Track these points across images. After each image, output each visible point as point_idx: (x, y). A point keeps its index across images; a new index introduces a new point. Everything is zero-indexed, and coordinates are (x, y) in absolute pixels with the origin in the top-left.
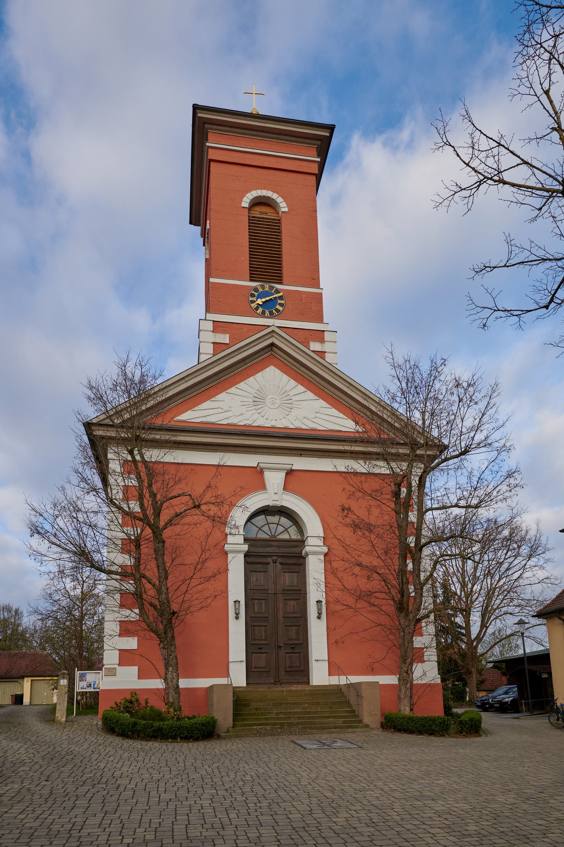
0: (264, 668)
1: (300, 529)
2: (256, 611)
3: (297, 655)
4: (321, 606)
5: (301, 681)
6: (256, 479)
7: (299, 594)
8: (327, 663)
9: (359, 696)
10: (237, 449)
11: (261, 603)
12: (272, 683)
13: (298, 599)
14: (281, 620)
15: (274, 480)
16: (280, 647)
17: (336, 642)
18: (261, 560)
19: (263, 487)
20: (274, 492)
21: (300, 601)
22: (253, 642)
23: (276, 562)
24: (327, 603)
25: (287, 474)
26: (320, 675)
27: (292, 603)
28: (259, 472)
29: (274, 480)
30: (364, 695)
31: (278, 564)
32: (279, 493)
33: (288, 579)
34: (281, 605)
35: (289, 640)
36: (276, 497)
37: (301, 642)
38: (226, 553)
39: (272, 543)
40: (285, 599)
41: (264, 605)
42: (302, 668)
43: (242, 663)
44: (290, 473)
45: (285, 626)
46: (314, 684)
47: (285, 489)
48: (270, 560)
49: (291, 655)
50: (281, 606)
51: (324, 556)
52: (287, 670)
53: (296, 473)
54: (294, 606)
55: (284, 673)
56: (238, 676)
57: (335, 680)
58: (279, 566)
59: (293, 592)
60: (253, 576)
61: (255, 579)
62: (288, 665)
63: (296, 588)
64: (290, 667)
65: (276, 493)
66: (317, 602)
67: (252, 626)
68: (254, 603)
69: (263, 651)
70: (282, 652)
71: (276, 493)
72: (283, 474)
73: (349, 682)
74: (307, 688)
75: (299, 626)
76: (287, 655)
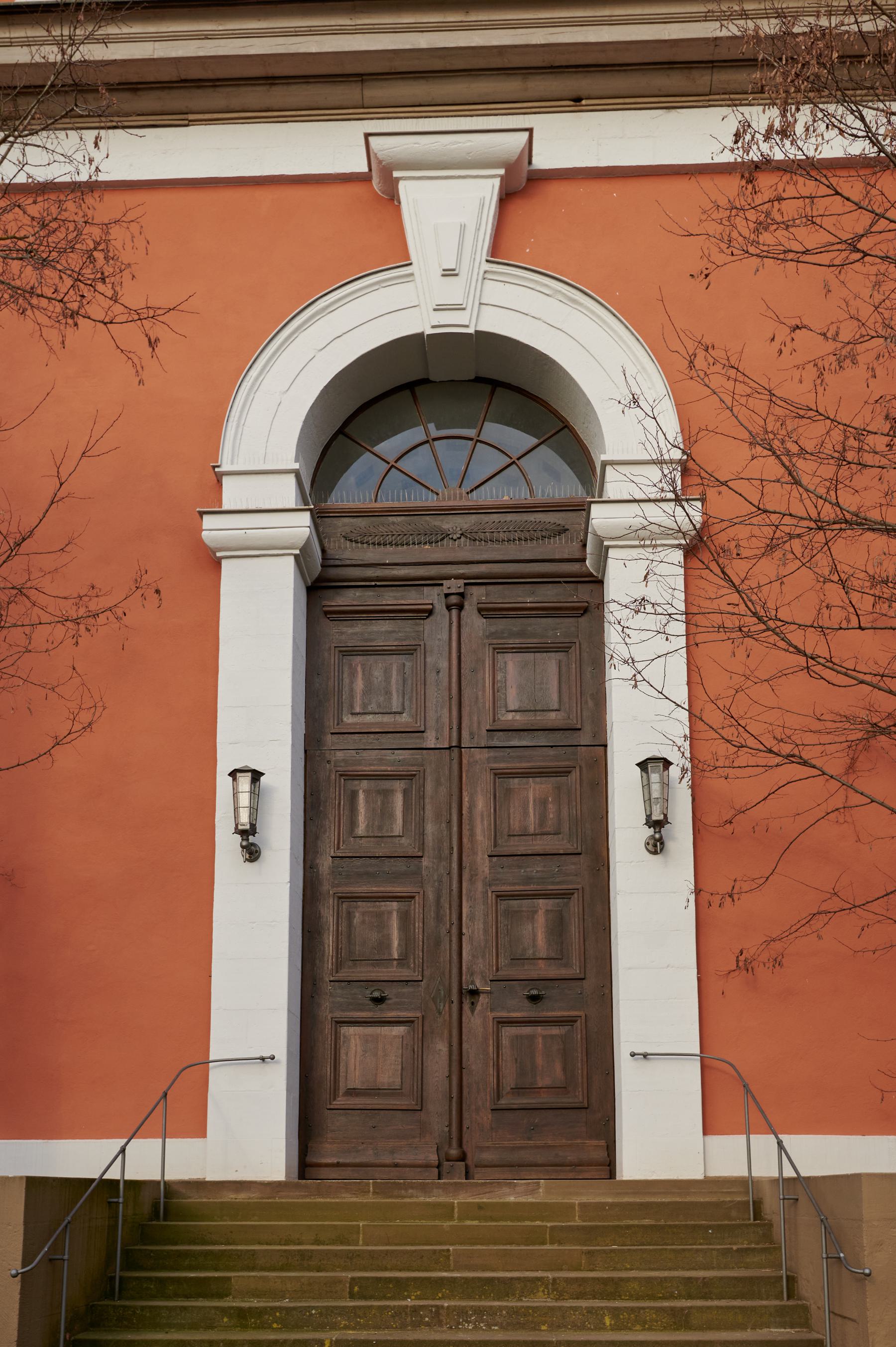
0: (392, 1092)
1: (584, 464)
2: (361, 829)
3: (555, 1031)
4: (665, 785)
5: (571, 1157)
6: (365, 220)
7: (573, 750)
8: (695, 1068)
9: (840, 1261)
10: (280, 95)
11: (387, 794)
12: (427, 1166)
13: (566, 772)
14: (484, 866)
15: (447, 212)
16: (475, 993)
17: (745, 965)
18: (389, 598)
19: (396, 254)
20: (445, 272)
21: (575, 775)
22: (343, 974)
23: (460, 607)
24: (698, 769)
25: (507, 197)
26: (661, 1130)
27: (534, 789)
28: (376, 191)
29: (447, 212)
30: (874, 1261)
31: (470, 608)
32: (464, 271)
33: (519, 685)
34: (480, 804)
35: (517, 960)
36: (453, 292)
37: (575, 970)
38: (211, 562)
39: (449, 524)
40: (499, 774)
41: (398, 801)
42: (578, 1097)
43: (269, 1067)
44: (521, 185)
45: (500, 896)
46: (624, 1179)
47: (498, 250)
48: (432, 597)
49: (527, 1030)
50: (480, 803)
51: (690, 552)
52: (503, 1102)
53: (555, 189)
54: (542, 803)
55: (486, 1117)
56: (243, 1133)
57: (735, 1157)
58: (475, 623)
59: (542, 739)
60: (353, 674)
61: (359, 685)
62: (509, 1080)
63: (552, 718)
64: (518, 1090)
65: (449, 273)
66: (643, 765)
67: (342, 898)
68: (354, 795)
69: (391, 1014)
70: (477, 1021)
71: (449, 273)
72: (488, 189)
73: (789, 1173)
74: (589, 1193)
75: (566, 895)
76: (508, 1032)
